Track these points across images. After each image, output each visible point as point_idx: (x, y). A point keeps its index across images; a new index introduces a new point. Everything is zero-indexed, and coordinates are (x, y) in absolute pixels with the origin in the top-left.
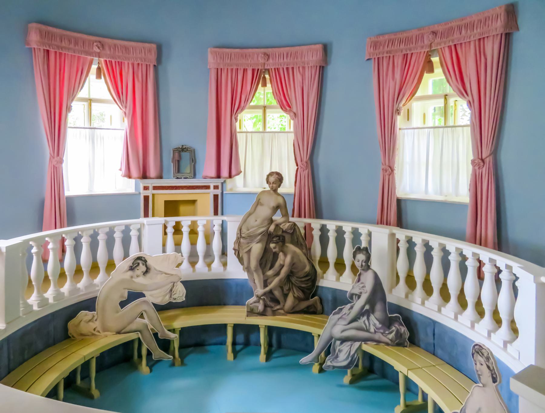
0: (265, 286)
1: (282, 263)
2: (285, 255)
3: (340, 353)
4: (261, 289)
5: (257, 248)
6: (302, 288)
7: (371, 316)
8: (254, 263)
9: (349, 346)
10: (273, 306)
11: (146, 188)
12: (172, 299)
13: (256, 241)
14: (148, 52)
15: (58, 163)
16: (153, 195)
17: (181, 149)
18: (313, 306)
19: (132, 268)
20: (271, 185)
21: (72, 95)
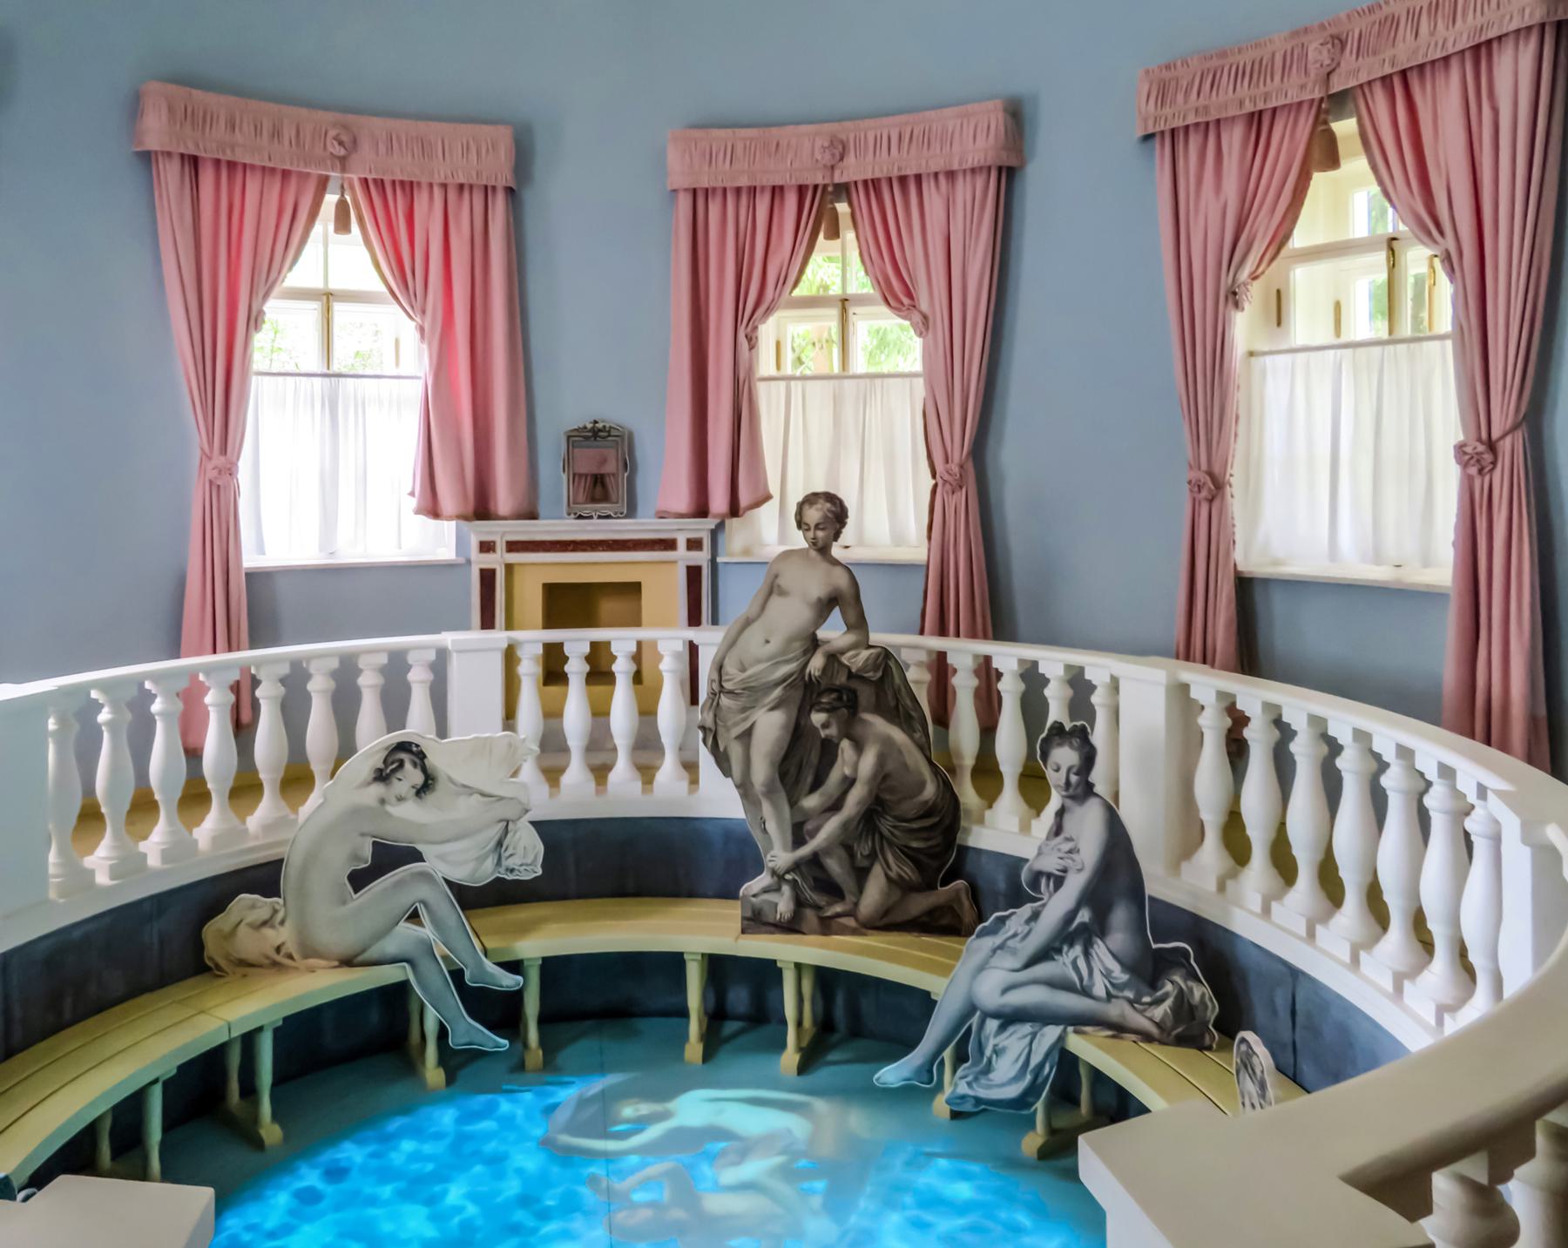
0: (799, 839)
1: (847, 771)
2: (859, 747)
3: (997, 1056)
4: (785, 849)
5: (770, 725)
6: (910, 852)
7: (1095, 946)
8: (761, 772)
9: (1025, 1037)
10: (823, 903)
11: (486, 547)
12: (502, 870)
13: (769, 703)
14: (488, 150)
15: (223, 472)
16: (509, 568)
17: (589, 432)
18: (949, 908)
19: (381, 774)
20: (811, 534)
21: (266, 278)
